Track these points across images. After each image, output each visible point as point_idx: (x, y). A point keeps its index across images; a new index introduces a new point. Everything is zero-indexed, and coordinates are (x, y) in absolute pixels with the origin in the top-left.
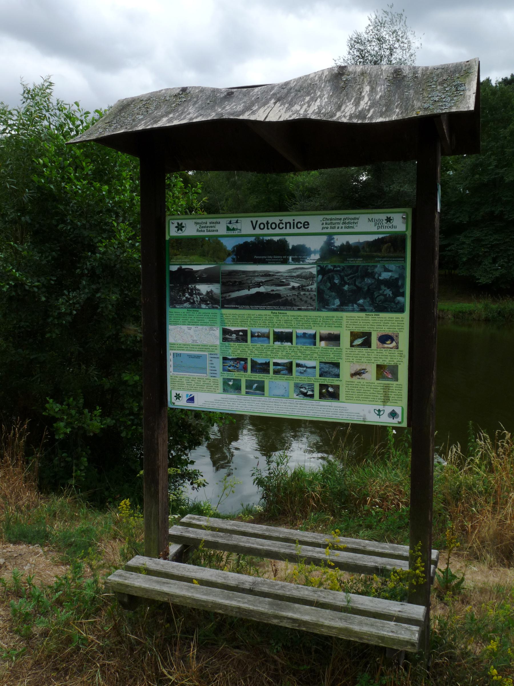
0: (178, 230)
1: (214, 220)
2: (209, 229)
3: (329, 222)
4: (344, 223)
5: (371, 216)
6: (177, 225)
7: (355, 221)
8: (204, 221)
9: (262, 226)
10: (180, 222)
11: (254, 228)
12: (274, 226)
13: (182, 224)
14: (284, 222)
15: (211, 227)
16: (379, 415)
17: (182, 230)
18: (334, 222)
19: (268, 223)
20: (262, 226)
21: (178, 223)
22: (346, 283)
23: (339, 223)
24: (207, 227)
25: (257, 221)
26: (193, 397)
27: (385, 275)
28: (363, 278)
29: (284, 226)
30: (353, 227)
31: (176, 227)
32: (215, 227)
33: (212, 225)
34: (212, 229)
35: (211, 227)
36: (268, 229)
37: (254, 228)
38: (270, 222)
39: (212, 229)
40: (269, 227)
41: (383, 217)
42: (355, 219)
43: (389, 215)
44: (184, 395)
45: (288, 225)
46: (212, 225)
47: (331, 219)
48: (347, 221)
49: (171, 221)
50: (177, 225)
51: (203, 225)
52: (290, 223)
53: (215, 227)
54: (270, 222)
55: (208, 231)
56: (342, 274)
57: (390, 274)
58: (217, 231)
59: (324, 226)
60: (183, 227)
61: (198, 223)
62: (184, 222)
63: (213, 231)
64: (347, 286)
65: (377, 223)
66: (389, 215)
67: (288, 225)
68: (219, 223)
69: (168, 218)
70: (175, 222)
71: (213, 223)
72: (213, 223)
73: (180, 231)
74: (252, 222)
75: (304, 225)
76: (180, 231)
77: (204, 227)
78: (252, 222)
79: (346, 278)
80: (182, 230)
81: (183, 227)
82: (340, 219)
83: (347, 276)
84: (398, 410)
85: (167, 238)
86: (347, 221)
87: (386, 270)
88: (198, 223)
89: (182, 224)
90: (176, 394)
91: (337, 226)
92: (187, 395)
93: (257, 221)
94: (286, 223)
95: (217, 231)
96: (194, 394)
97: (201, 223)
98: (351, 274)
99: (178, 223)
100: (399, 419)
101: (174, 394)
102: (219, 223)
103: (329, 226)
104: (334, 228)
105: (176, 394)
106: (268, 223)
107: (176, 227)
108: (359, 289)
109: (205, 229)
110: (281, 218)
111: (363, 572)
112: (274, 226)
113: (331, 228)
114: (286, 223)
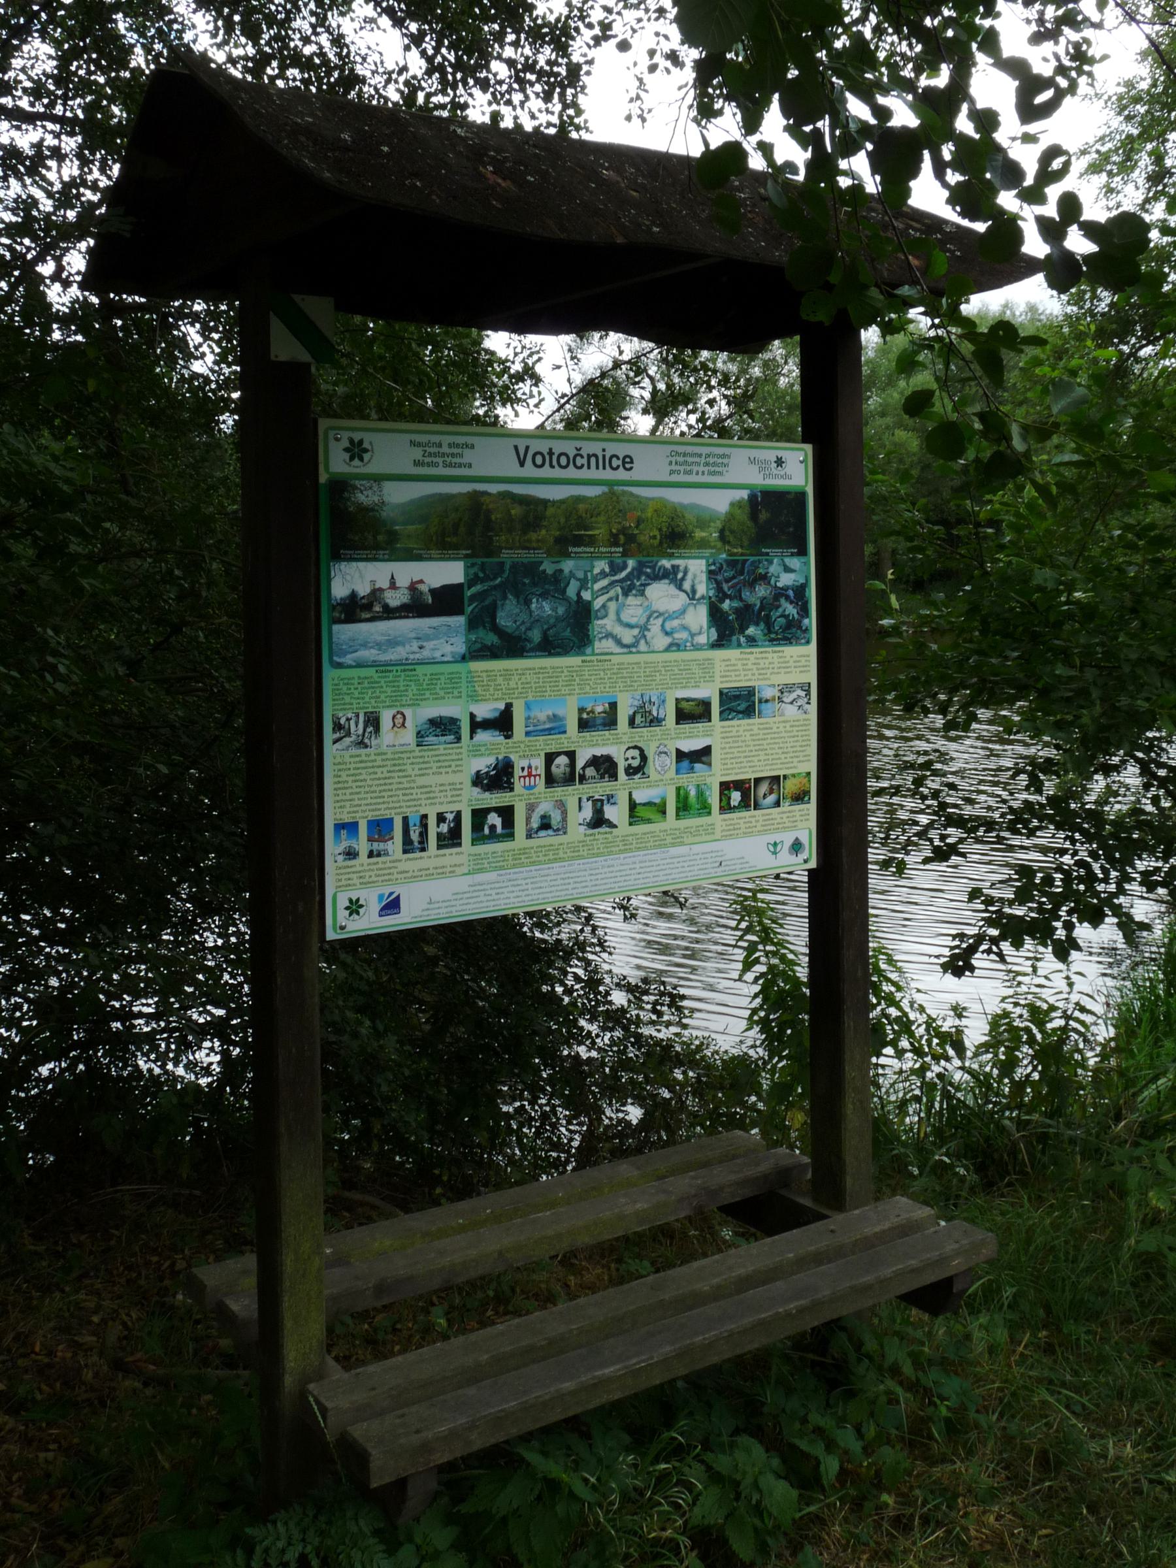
0: (352, 458)
1: (461, 440)
2: (448, 460)
3: (681, 459)
4: (707, 464)
5: (753, 453)
6: (347, 444)
7: (725, 461)
8: (435, 438)
9: (539, 460)
10: (357, 436)
11: (522, 464)
12: (563, 461)
13: (361, 442)
14: (584, 452)
15: (453, 455)
16: (775, 853)
17: (361, 459)
18: (690, 460)
19: (551, 453)
20: (539, 460)
21: (351, 441)
22: (726, 596)
23: (699, 464)
24: (443, 455)
25: (527, 448)
26: (398, 897)
27: (786, 580)
28: (752, 585)
29: (585, 461)
30: (721, 473)
31: (346, 450)
32: (461, 456)
33: (455, 451)
34: (458, 460)
35: (453, 455)
36: (552, 466)
37: (522, 464)
38: (557, 451)
39: (458, 460)
40: (555, 463)
41: (771, 455)
42: (724, 456)
43: (780, 453)
44: (372, 901)
45: (593, 460)
46: (455, 451)
47: (685, 455)
48: (711, 460)
49: (331, 434)
50: (347, 444)
51: (432, 450)
52: (596, 456)
53: (461, 456)
54: (557, 451)
55: (446, 465)
56: (719, 578)
57: (792, 576)
58: (470, 466)
59: (674, 467)
60: (366, 451)
61: (419, 445)
62: (368, 438)
63: (460, 465)
64: (727, 601)
65: (762, 465)
66: (780, 453)
67: (593, 460)
68: (473, 447)
69: (323, 424)
70: (345, 436)
71: (458, 446)
72: (458, 446)
73: (356, 462)
74: (516, 448)
75: (624, 463)
76: (356, 462)
77: (435, 455)
78: (516, 448)
79: (725, 587)
80: (361, 459)
81: (366, 451)
82: (700, 456)
83: (727, 581)
84: (805, 840)
85: (323, 478)
86: (711, 460)
87: (787, 570)
88: (419, 445)
89: (361, 442)
90: (351, 901)
91: (695, 469)
92: (381, 897)
93: (527, 448)
94: (589, 456)
95: (470, 466)
96: (398, 890)
97: (427, 444)
98: (734, 577)
99: (351, 441)
100: (805, 856)
101: (343, 902)
102: (473, 447)
103: (682, 468)
104: (689, 472)
105: (351, 901)
106: (551, 453)
107: (346, 450)
108: (748, 607)
109: (440, 460)
110: (578, 444)
111: (816, 1156)
112: (563, 461)
113: (686, 472)
114: (589, 456)
